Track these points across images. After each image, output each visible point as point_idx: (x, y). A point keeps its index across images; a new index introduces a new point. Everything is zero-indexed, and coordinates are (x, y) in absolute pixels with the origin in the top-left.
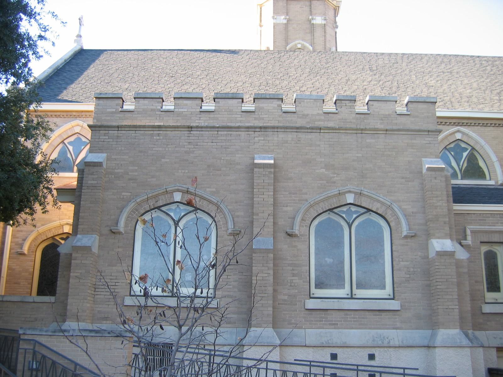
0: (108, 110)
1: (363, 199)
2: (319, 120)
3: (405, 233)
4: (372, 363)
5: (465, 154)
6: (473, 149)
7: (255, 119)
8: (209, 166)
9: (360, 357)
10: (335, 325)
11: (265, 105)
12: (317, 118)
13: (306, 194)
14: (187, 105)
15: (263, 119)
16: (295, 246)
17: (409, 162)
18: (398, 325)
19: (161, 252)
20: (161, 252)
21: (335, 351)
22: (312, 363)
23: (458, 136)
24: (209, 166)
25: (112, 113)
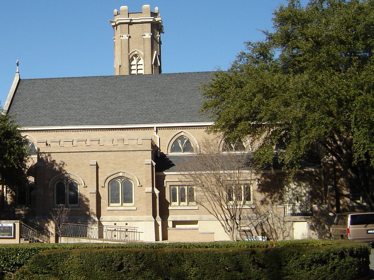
0: (42, 146)
1: (125, 174)
2: (111, 148)
3: (138, 186)
4: (127, 226)
5: (185, 141)
6: (188, 139)
7: (90, 148)
8: (76, 165)
9: (123, 224)
10: (116, 215)
11: (93, 143)
12: (111, 147)
13: (107, 173)
14: (67, 144)
15: (92, 148)
16: (104, 191)
17: (141, 161)
18: (136, 214)
19: (120, 72)
20: (120, 72)
21: (115, 222)
22: (121, 228)
23: (182, 134)
24: (76, 165)
25: (43, 147)
